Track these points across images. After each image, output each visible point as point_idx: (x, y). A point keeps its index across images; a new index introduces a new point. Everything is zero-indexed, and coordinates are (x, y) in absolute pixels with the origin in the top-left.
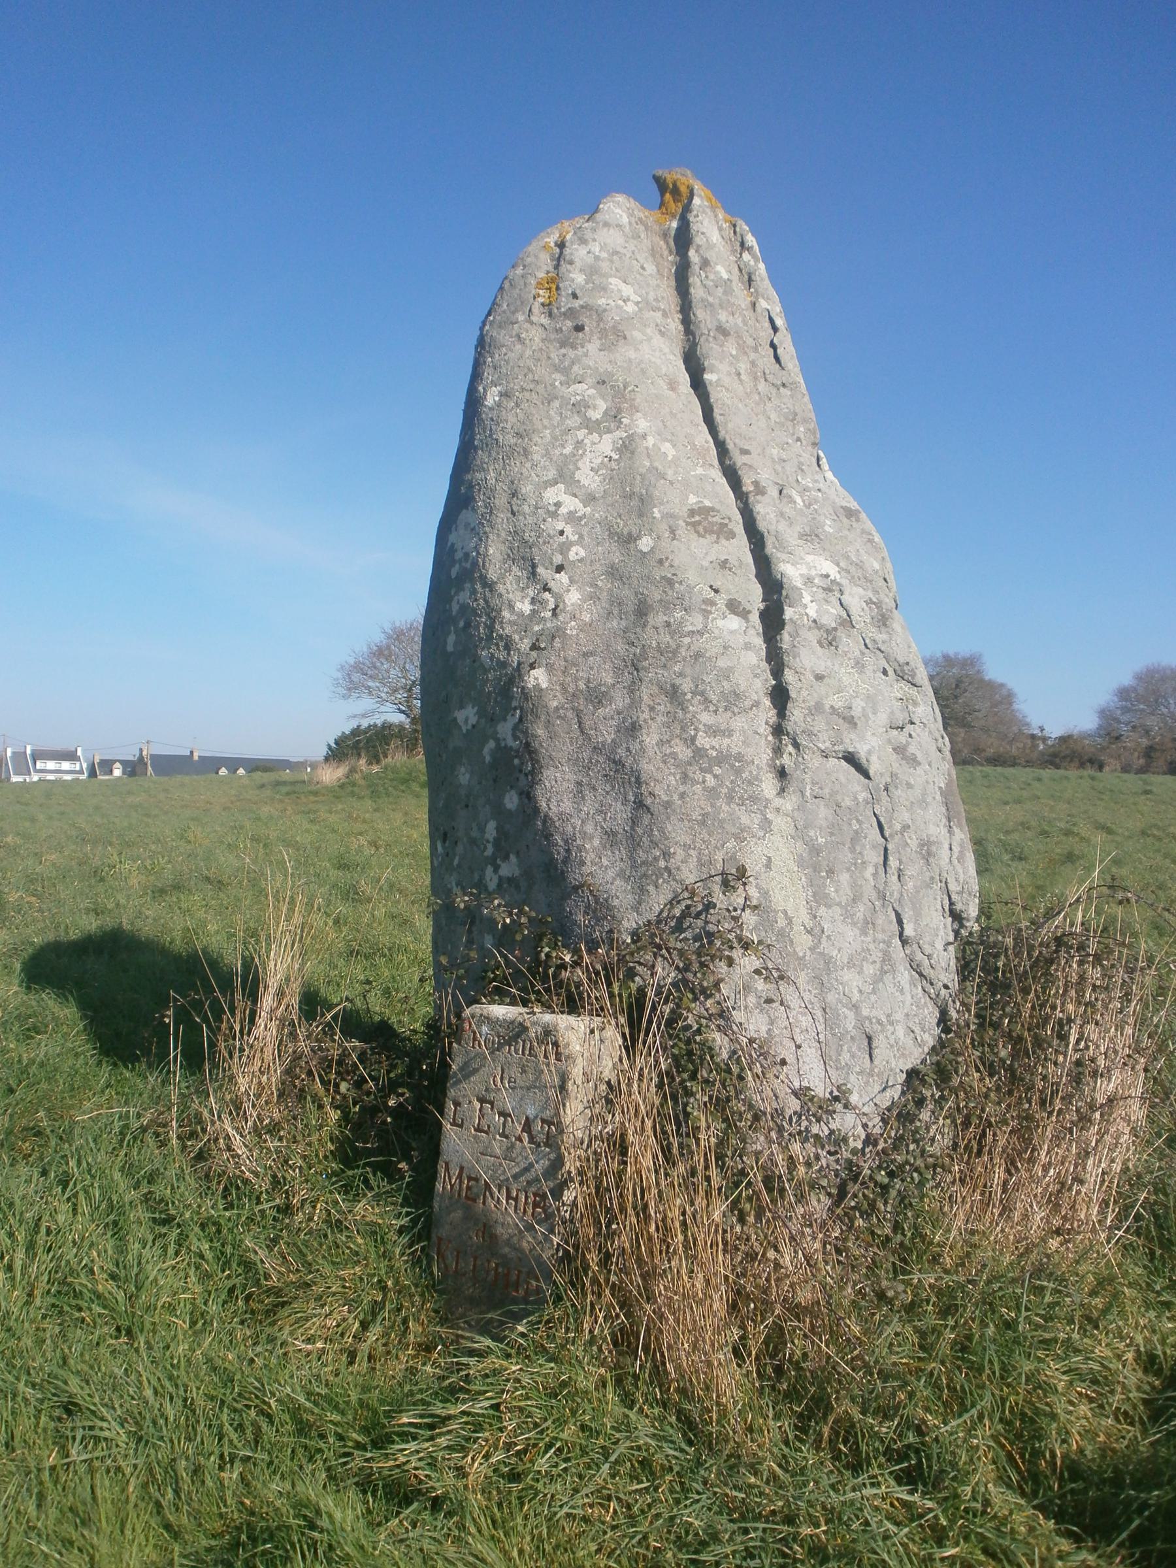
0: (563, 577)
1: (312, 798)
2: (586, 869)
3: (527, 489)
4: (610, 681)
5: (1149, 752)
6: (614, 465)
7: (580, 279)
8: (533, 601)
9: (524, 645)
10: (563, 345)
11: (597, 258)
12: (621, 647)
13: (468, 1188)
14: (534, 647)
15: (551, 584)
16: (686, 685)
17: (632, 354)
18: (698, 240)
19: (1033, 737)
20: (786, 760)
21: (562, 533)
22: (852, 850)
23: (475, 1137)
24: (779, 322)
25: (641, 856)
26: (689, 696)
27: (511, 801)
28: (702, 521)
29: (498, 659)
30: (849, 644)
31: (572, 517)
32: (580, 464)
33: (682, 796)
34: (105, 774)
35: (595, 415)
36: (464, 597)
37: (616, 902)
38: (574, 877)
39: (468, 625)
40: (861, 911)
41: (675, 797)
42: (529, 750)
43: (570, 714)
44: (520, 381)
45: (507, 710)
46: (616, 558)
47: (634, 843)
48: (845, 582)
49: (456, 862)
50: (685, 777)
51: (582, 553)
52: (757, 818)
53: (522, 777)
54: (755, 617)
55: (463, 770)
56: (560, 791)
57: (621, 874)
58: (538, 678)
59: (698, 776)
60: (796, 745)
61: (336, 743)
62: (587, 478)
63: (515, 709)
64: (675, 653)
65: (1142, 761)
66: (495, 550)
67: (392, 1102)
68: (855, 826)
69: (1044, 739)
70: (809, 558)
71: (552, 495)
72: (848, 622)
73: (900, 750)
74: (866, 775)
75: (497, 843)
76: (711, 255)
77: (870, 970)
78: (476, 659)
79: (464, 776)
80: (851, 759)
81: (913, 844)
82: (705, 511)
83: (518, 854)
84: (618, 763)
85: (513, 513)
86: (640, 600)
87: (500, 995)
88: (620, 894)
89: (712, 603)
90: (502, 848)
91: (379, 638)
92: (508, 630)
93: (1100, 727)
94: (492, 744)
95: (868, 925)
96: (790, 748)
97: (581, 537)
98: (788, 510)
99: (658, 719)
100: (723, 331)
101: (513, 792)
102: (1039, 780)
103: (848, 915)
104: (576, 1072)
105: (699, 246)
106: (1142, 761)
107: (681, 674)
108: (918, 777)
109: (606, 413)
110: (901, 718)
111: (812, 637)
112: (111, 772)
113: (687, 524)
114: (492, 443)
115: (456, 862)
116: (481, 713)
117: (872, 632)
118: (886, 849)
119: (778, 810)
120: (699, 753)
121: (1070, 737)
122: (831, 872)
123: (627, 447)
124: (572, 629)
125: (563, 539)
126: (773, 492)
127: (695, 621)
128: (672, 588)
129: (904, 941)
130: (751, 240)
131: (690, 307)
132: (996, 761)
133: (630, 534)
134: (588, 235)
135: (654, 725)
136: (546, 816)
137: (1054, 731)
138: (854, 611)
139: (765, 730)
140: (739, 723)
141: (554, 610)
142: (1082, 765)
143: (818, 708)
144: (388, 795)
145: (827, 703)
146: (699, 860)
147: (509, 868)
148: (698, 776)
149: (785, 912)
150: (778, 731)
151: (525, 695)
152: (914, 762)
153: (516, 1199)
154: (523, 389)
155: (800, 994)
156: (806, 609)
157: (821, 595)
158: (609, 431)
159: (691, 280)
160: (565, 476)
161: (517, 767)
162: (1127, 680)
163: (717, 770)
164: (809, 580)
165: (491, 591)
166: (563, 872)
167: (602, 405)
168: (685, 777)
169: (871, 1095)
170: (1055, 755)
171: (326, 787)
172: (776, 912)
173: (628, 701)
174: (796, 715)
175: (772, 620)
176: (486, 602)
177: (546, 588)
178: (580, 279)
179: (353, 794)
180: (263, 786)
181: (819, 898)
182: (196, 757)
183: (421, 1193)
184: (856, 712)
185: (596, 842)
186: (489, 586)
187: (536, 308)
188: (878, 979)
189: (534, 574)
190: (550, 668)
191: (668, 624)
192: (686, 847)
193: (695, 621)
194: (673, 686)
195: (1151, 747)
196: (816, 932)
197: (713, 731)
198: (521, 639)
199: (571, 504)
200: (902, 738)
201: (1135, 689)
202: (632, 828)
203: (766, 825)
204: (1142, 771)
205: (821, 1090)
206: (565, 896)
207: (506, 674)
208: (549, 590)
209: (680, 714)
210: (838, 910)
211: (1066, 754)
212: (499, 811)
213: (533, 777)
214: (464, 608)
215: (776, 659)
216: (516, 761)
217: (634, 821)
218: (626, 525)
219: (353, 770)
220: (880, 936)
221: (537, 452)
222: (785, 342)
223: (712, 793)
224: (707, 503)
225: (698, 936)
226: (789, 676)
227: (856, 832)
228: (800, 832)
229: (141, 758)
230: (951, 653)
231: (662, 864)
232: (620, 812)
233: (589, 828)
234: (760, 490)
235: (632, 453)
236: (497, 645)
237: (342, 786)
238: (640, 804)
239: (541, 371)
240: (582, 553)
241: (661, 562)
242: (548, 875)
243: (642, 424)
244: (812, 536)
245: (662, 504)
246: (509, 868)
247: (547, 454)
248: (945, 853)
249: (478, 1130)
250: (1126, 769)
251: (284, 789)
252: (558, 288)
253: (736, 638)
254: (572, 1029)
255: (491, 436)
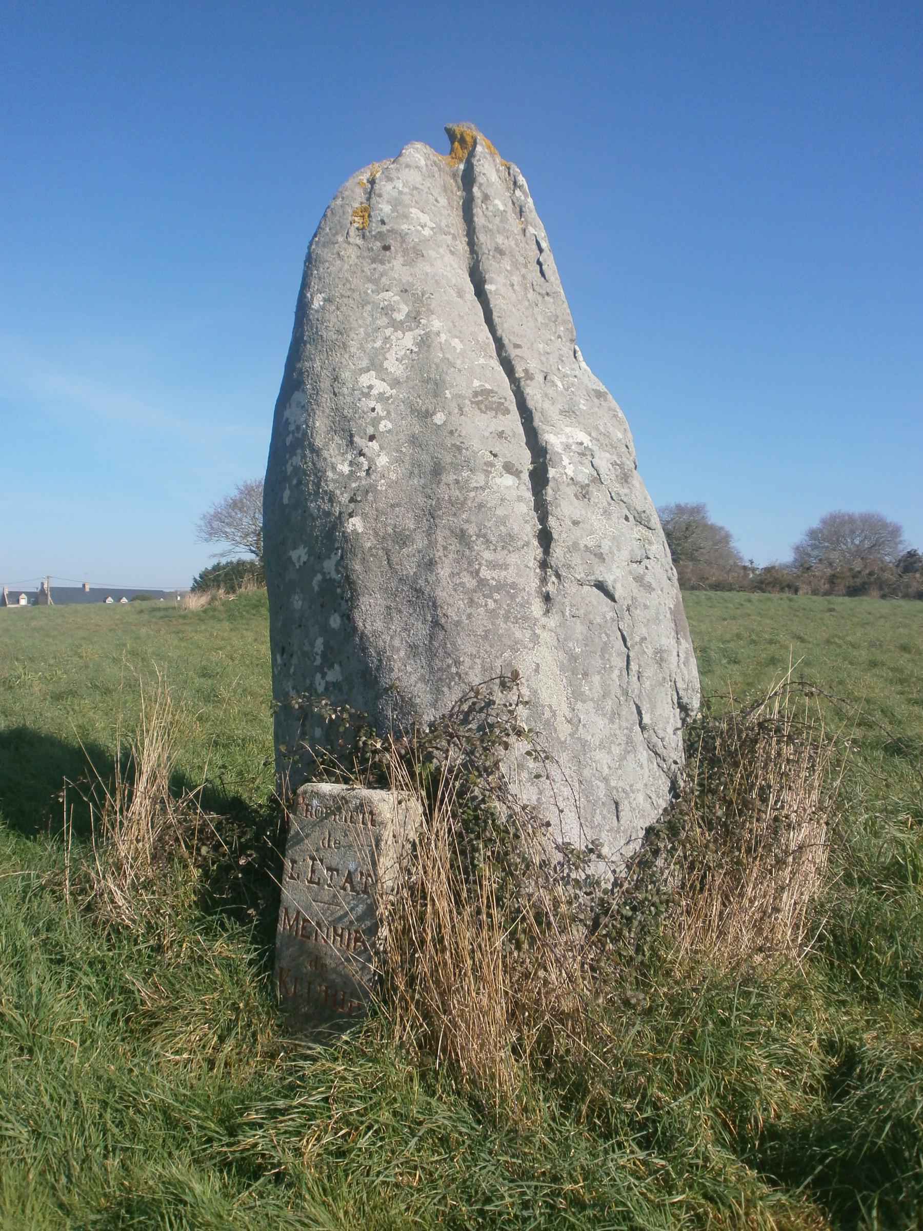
0: (375, 445)
1: (181, 621)
2: (394, 675)
3: (346, 375)
4: (412, 527)
5: (832, 580)
6: (414, 356)
7: (387, 209)
8: (351, 464)
9: (344, 498)
10: (374, 261)
11: (400, 192)
12: (420, 500)
13: (304, 928)
14: (352, 500)
15: (365, 450)
16: (472, 530)
17: (428, 269)
18: (481, 179)
19: (745, 568)
20: (550, 588)
21: (373, 410)
22: (602, 657)
23: (308, 888)
24: (544, 245)
25: (437, 664)
26: (474, 538)
27: (335, 622)
28: (484, 400)
29: (324, 510)
30: (599, 496)
31: (381, 397)
32: (388, 355)
33: (469, 616)
34: (13, 603)
35: (400, 316)
36: (296, 460)
37: (418, 701)
38: (385, 682)
39: (300, 483)
40: (609, 704)
41: (464, 617)
42: (349, 582)
43: (380, 552)
44: (340, 289)
45: (331, 550)
46: (417, 430)
47: (431, 654)
48: (595, 448)
49: (292, 670)
50: (471, 602)
51: (390, 426)
52: (528, 634)
53: (343, 603)
54: (525, 476)
55: (296, 597)
56: (373, 614)
57: (422, 679)
58: (355, 524)
59: (482, 601)
60: (558, 576)
61: (201, 577)
62: (393, 366)
63: (337, 549)
64: (463, 504)
65: (827, 586)
66: (320, 423)
67: (242, 861)
68: (605, 639)
69: (753, 570)
70: (568, 430)
71: (366, 380)
72: (598, 479)
73: (639, 579)
74: (612, 598)
75: (324, 655)
76: (490, 192)
77: (616, 750)
78: (306, 509)
79: (297, 603)
80: (600, 586)
81: (650, 652)
82: (486, 393)
83: (341, 665)
84: (419, 591)
85: (335, 394)
86: (435, 463)
87: (330, 775)
88: (421, 694)
89: (492, 465)
90: (328, 659)
91: (234, 493)
92: (331, 486)
93: (796, 560)
94: (319, 577)
95: (614, 716)
96: (554, 579)
97: (389, 413)
98: (551, 392)
99: (450, 556)
100: (500, 251)
101: (336, 615)
102: (750, 601)
103: (599, 708)
104: (387, 835)
105: (481, 184)
106: (827, 586)
107: (467, 521)
108: (653, 600)
109: (408, 315)
110: (639, 554)
111: (570, 491)
112: (18, 602)
113: (472, 403)
114: (317, 339)
115: (292, 670)
116: (310, 553)
117: (617, 488)
118: (628, 657)
119: (544, 627)
120: (482, 583)
121: (773, 568)
122: (585, 675)
123: (424, 342)
124: (382, 485)
125: (374, 414)
126: (539, 378)
127: (478, 480)
128: (460, 453)
129: (643, 728)
130: (521, 180)
131: (474, 232)
132: (717, 587)
133: (427, 411)
134: (394, 174)
135: (447, 561)
136: (363, 633)
137: (762, 563)
138: (602, 471)
139: (533, 564)
140: (513, 559)
141: (368, 471)
142: (782, 590)
143: (575, 546)
144: (242, 617)
145: (582, 543)
146: (483, 667)
147: (334, 675)
148: (482, 601)
149: (550, 707)
150: (544, 565)
151: (345, 536)
152: (649, 588)
153: (341, 936)
154: (342, 296)
155: (563, 768)
156: (565, 469)
157: (577, 458)
158: (411, 330)
159: (475, 211)
160: (376, 365)
161: (339, 595)
162: (815, 524)
163: (497, 596)
164: (567, 447)
165: (318, 456)
166: (376, 677)
167: (405, 309)
168: (471, 602)
169: (618, 847)
170: (762, 582)
171: (193, 612)
172: (543, 706)
173: (426, 542)
174: (558, 552)
175: (539, 478)
176: (314, 464)
177: (361, 454)
178: (387, 209)
179: (213, 617)
180: (141, 612)
181: (577, 695)
182: (87, 589)
183: (266, 934)
184: (605, 550)
185: (402, 653)
186: (316, 451)
187: (352, 232)
188: (623, 758)
189: (351, 442)
190: (365, 517)
191: (457, 482)
192: (472, 657)
193: (478, 480)
194: (462, 530)
195: (834, 575)
196: (574, 722)
197: (493, 566)
198: (342, 494)
199: (380, 387)
200: (640, 569)
201: (821, 531)
202: (430, 642)
203: (535, 638)
204: (827, 593)
205: (579, 844)
206: (378, 697)
207: (330, 522)
208: (364, 455)
209: (467, 552)
210: (591, 704)
211: (770, 581)
212: (325, 629)
213: (352, 603)
214: (297, 469)
215: (542, 509)
216: (339, 590)
217: (432, 637)
218: (424, 403)
219: (214, 598)
220: (624, 724)
221: (354, 346)
222: (550, 266)
223: (492, 614)
224: (488, 386)
225: (481, 726)
226: (552, 522)
227: (605, 643)
228: (561, 644)
229: (43, 589)
230: (682, 504)
231: (454, 670)
232: (421, 630)
233: (397, 643)
234: (529, 376)
235: (429, 347)
236: (323, 498)
237: (205, 611)
238: (436, 624)
239: (356, 282)
240: (390, 426)
241: (451, 432)
242: (365, 681)
243: (436, 324)
244: (569, 412)
245: (452, 386)
246: (334, 675)
247: (361, 347)
248: (673, 659)
249: (310, 882)
250: (815, 592)
251: (159, 614)
252: (369, 216)
253: (511, 492)
254: (384, 801)
255: (317, 333)
